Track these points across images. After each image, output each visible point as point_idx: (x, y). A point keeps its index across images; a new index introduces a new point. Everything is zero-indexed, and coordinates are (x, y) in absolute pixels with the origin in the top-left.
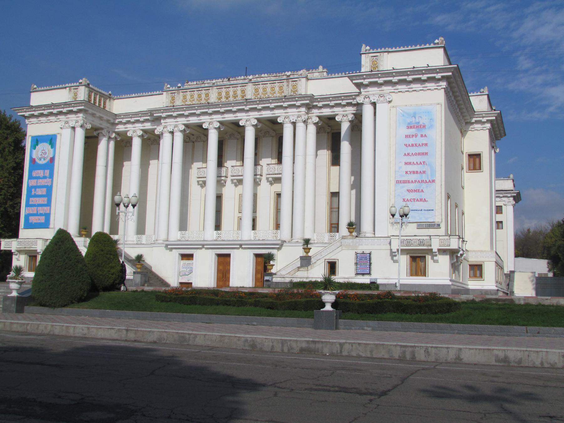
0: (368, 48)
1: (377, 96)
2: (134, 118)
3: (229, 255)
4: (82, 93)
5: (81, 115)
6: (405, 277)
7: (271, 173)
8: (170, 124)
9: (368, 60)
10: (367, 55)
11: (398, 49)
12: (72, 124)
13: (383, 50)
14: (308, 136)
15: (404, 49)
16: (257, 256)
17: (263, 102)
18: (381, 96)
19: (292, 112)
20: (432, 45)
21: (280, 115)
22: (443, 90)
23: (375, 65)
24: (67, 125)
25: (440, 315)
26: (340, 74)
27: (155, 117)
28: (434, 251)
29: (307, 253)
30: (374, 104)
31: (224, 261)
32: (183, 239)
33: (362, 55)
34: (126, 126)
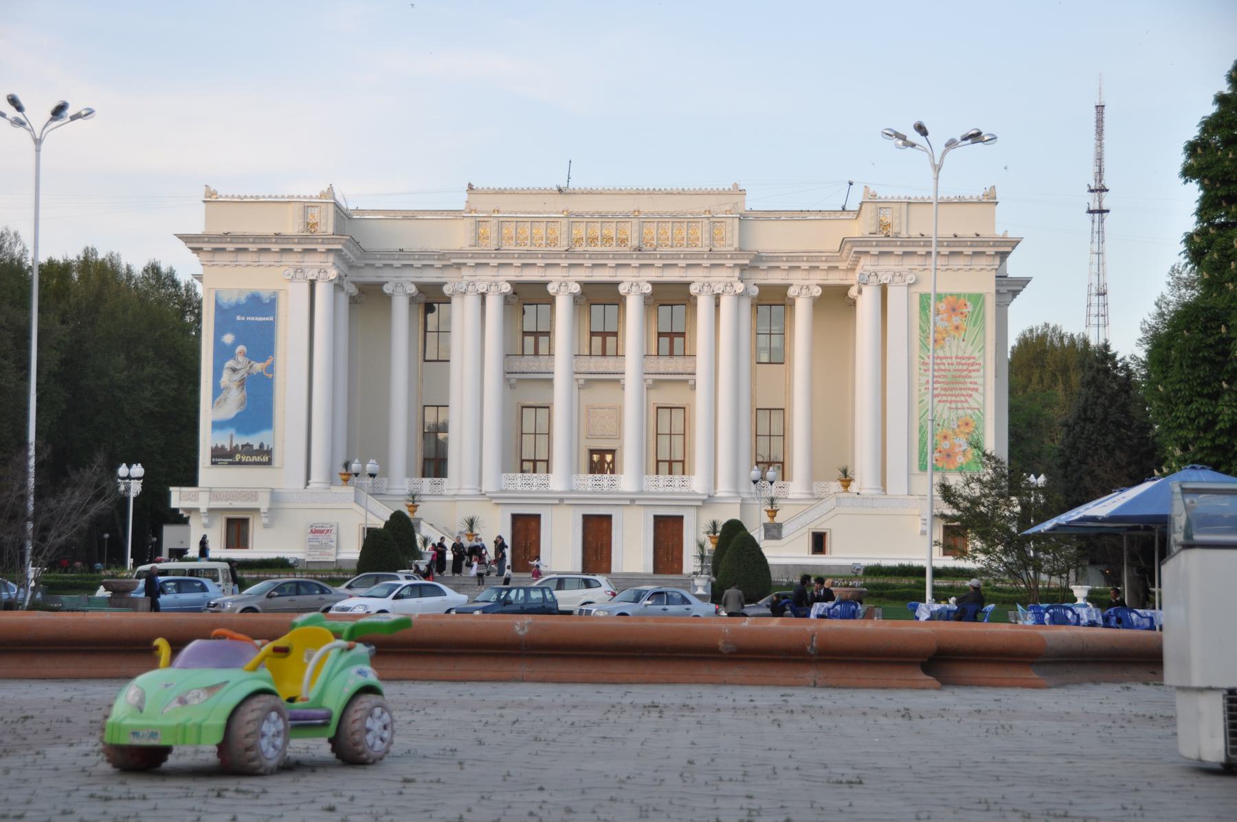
5: (331, 258)
8: (483, 280)
30: (884, 289)
34: (380, 273)
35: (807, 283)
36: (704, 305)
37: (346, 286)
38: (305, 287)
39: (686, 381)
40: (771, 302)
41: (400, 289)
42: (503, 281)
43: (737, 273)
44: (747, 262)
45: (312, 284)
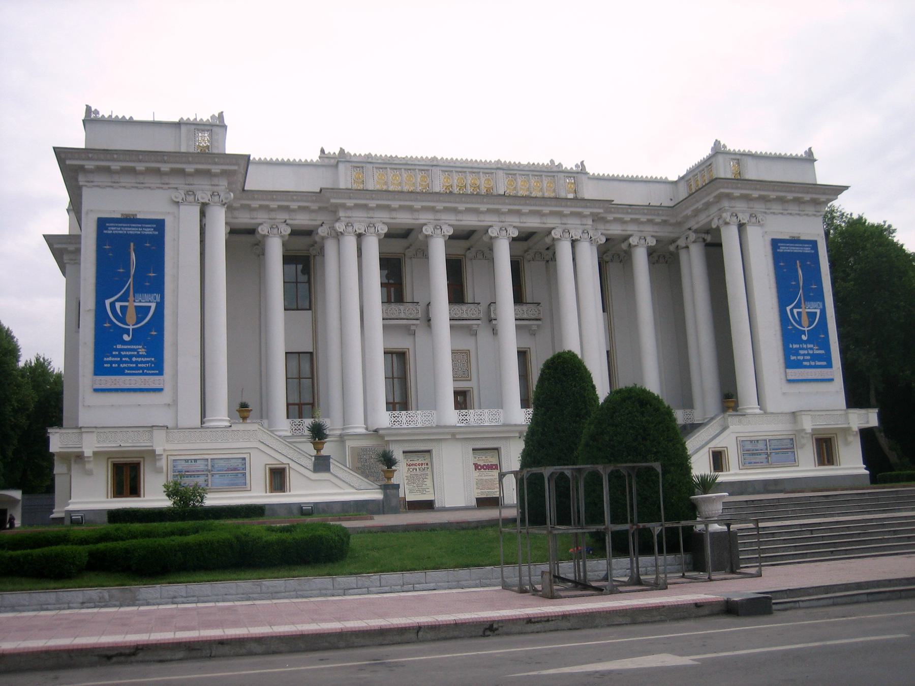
6: (105, 499)
14: (589, 258)
24: (191, 198)
32: (397, 426)
35: (643, 234)
36: (564, 250)
37: (445, 228)
38: (196, 210)
39: (469, 327)
40: (613, 258)
41: (350, 229)
42: (382, 223)
43: (590, 222)
44: (601, 211)
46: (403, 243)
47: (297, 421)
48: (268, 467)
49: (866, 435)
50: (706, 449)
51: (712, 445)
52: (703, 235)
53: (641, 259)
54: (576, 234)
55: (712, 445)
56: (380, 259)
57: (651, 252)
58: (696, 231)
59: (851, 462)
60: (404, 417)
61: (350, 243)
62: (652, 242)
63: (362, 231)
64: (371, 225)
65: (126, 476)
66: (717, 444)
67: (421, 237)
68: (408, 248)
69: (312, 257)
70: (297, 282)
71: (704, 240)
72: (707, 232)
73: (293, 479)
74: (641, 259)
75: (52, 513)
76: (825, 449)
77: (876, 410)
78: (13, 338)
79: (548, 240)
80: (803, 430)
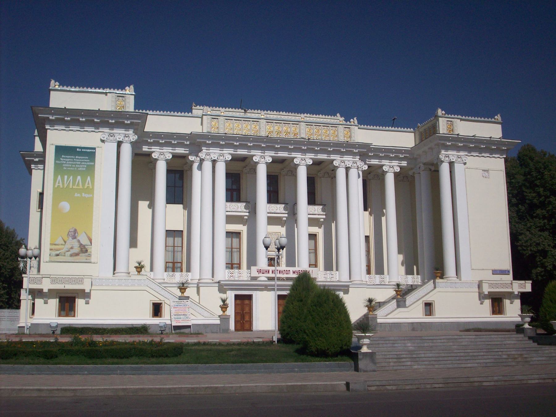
0: (443, 112)
1: (123, 135)
2: (167, 139)
3: (250, 297)
4: (130, 106)
6: (54, 318)
7: (234, 210)
8: (215, 153)
9: (445, 123)
10: (444, 119)
11: (97, 90)
12: (120, 138)
13: (456, 116)
15: (95, 91)
16: (280, 297)
17: (324, 147)
18: (459, 157)
19: (349, 160)
20: (493, 120)
21: (337, 160)
22: (503, 159)
23: (451, 128)
25: (160, 359)
26: (179, 113)
27: (196, 142)
28: (86, 291)
29: (183, 293)
31: (244, 303)
32: (232, 279)
33: (440, 119)
36: (341, 174)
45: (119, 144)
46: (242, 164)
47: (171, 273)
48: (152, 302)
49: (524, 297)
50: (421, 301)
51: (424, 299)
52: (430, 167)
53: (390, 180)
54: (349, 164)
55: (424, 299)
56: (226, 174)
57: (396, 175)
58: (424, 164)
59: (513, 312)
60: (237, 273)
61: (207, 165)
62: (398, 169)
63: (216, 158)
64: (223, 155)
65: (67, 302)
66: (428, 299)
67: (252, 163)
68: (245, 167)
69: (185, 172)
70: (175, 187)
71: (430, 170)
72: (432, 164)
73: (166, 310)
74: (390, 180)
75: (19, 323)
76: (497, 302)
77: (35, 151)
78: (344, 304)
79: (331, 167)
80: (513, 292)
